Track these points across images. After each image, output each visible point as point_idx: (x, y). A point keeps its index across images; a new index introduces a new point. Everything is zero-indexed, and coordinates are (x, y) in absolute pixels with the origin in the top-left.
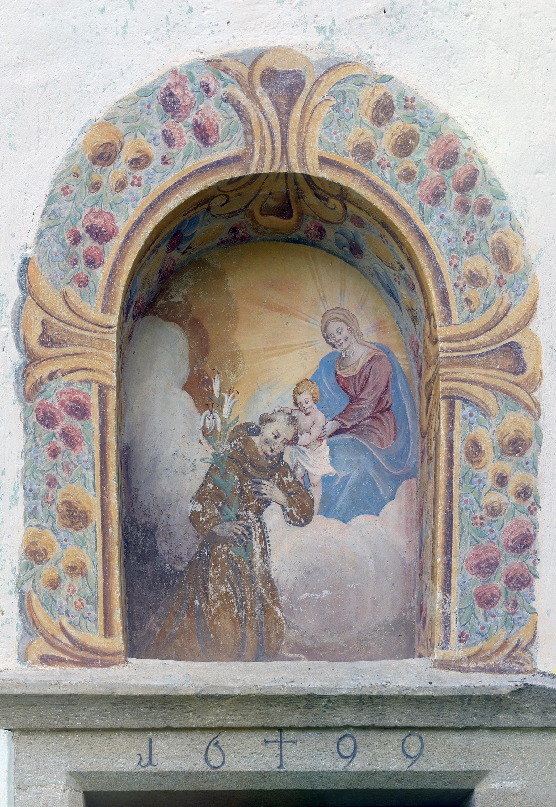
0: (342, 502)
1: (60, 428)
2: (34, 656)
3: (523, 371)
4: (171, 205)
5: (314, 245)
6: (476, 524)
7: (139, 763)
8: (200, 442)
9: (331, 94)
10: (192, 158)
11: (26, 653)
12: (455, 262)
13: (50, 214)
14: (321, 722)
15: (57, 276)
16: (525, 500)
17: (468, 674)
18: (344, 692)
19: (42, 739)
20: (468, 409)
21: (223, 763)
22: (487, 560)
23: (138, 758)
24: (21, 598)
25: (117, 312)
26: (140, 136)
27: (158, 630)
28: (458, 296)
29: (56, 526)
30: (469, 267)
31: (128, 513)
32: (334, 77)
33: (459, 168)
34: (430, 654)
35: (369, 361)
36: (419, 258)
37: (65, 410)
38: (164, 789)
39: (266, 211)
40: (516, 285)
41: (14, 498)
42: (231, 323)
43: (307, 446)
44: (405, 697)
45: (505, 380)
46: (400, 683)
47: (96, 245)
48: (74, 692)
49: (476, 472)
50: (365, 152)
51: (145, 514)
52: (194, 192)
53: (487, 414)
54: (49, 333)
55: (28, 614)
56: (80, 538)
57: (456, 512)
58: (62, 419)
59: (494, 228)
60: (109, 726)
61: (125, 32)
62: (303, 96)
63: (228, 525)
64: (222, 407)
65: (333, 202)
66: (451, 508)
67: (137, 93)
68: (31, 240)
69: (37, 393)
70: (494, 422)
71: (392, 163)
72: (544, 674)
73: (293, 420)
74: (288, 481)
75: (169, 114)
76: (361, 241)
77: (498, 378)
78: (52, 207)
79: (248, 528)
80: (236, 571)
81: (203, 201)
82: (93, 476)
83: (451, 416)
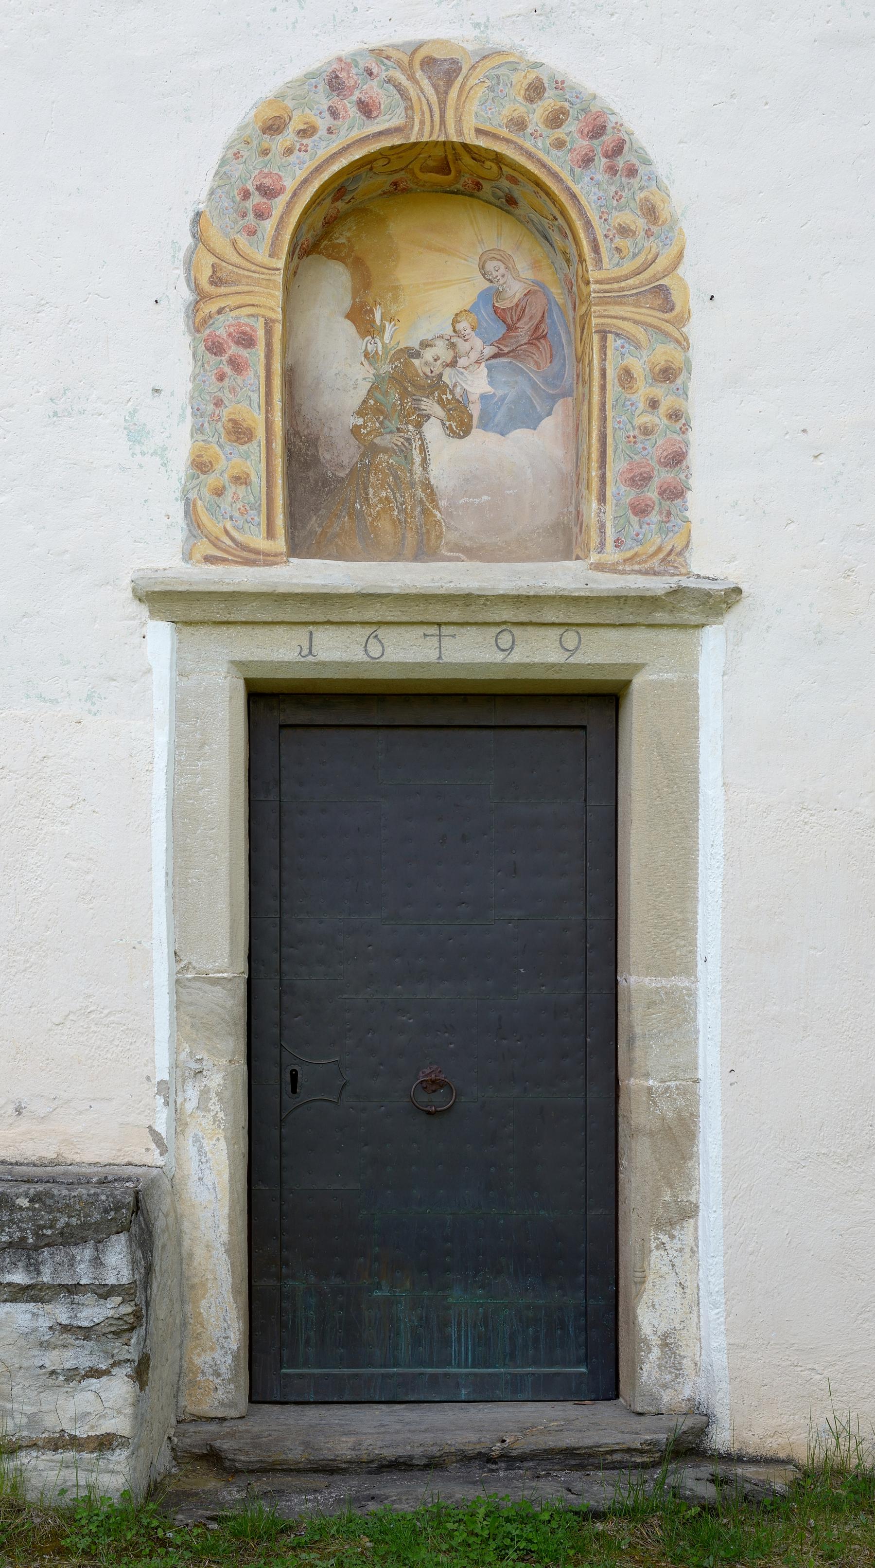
0: (500, 417)
1: (227, 355)
2: (198, 556)
3: (672, 309)
4: (335, 168)
5: (471, 196)
6: (630, 442)
7: (300, 653)
8: (362, 364)
9: (486, 77)
10: (355, 129)
11: (190, 554)
12: (605, 216)
13: (222, 175)
14: (480, 618)
15: (227, 226)
16: (676, 421)
17: (624, 576)
18: (501, 592)
19: (203, 630)
20: (620, 342)
21: (383, 654)
22: (641, 474)
23: (299, 649)
24: (187, 504)
25: (284, 257)
26: (307, 110)
27: (319, 530)
28: (609, 245)
29: (222, 441)
30: (618, 220)
31: (292, 426)
32: (488, 64)
33: (608, 139)
34: (587, 557)
35: (525, 295)
36: (571, 212)
37: (232, 340)
38: (324, 677)
39: (425, 169)
40: (663, 237)
41: (182, 417)
42: (393, 261)
43: (465, 368)
44: (561, 596)
45: (655, 317)
46: (556, 585)
47: (265, 200)
48: (237, 589)
49: (628, 396)
50: (519, 125)
51: (308, 427)
52: (357, 157)
53: (638, 346)
54: (218, 274)
55: (193, 518)
56: (245, 452)
57: (609, 431)
58: (230, 348)
59: (641, 189)
60: (270, 619)
61: (294, 27)
62: (460, 79)
63: (388, 436)
64: (383, 333)
65: (488, 164)
66: (605, 428)
67: (305, 76)
68: (204, 196)
69: (206, 326)
70: (644, 353)
71: (544, 134)
72: (698, 576)
73: (452, 346)
74: (447, 398)
75: (335, 93)
76: (516, 194)
77: (648, 315)
78: (224, 169)
79: (408, 440)
80: (396, 478)
81: (367, 163)
82: (258, 397)
83: (603, 348)
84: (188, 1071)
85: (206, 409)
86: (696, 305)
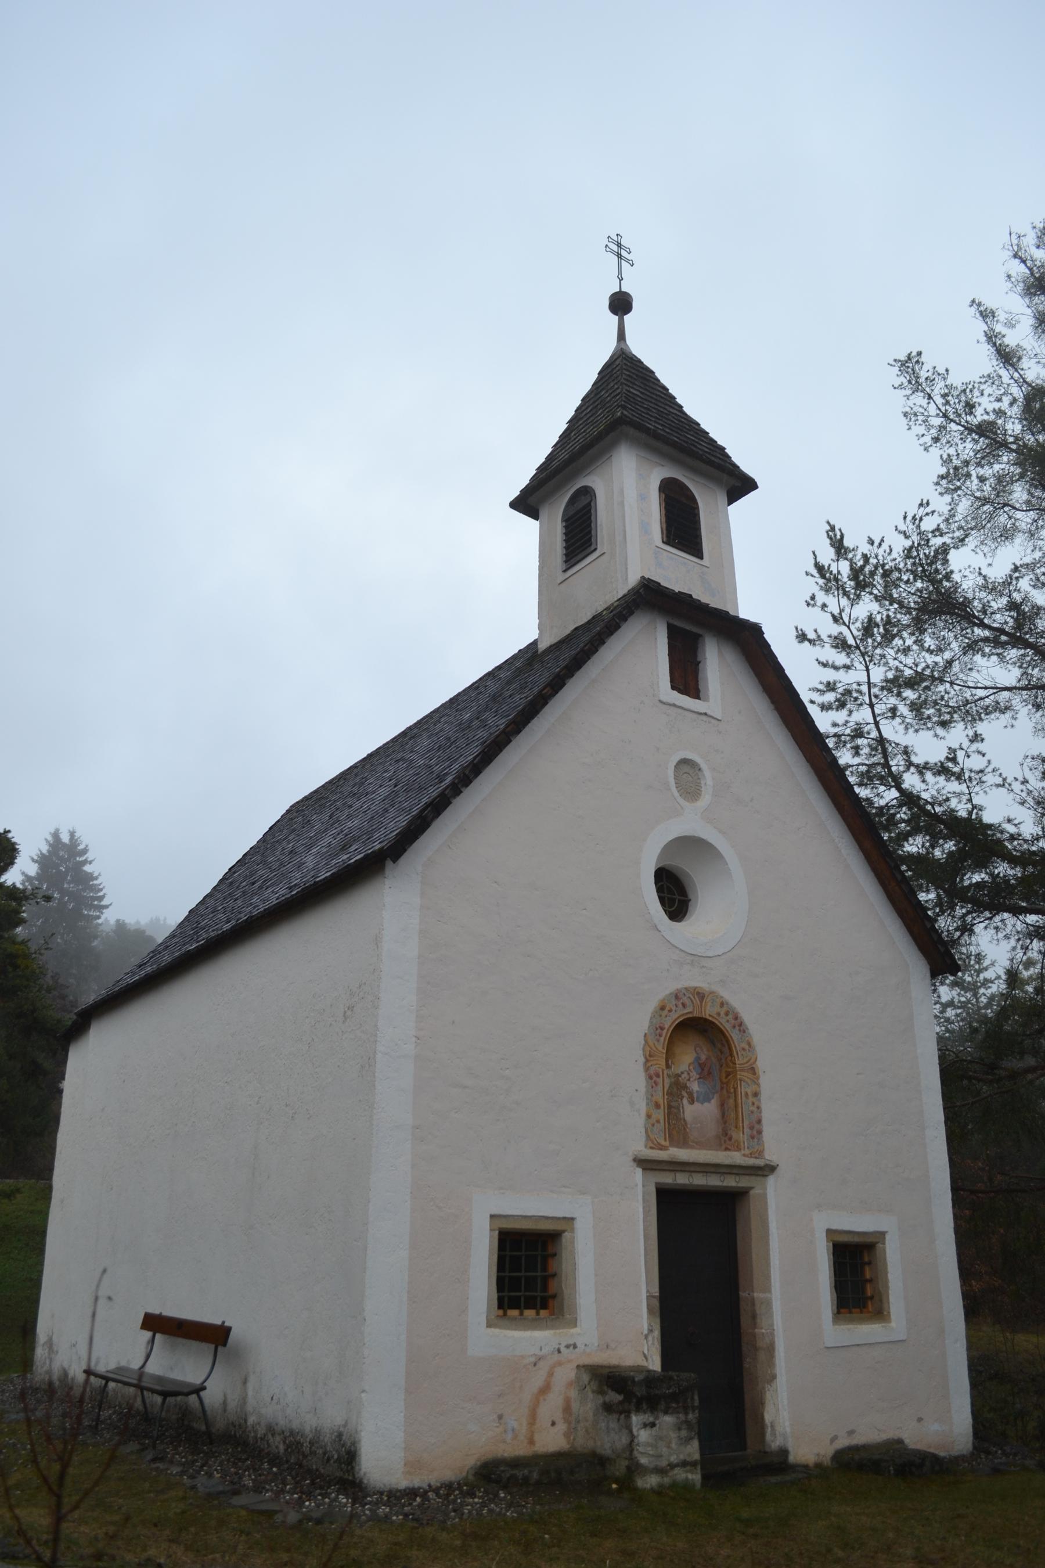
13: (651, 1022)
50: (719, 1014)
82: (661, 1094)
84: (651, 1331)
85: (650, 1096)
86: (761, 1073)
